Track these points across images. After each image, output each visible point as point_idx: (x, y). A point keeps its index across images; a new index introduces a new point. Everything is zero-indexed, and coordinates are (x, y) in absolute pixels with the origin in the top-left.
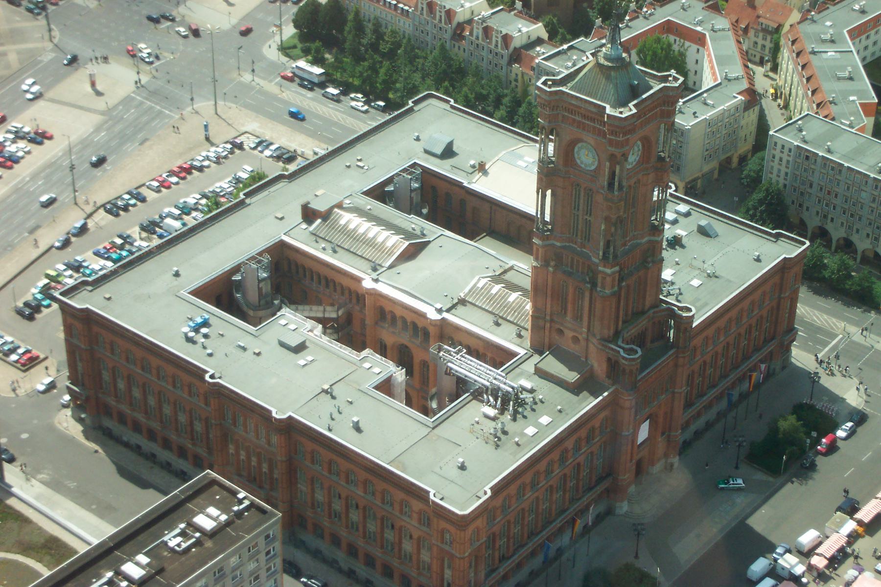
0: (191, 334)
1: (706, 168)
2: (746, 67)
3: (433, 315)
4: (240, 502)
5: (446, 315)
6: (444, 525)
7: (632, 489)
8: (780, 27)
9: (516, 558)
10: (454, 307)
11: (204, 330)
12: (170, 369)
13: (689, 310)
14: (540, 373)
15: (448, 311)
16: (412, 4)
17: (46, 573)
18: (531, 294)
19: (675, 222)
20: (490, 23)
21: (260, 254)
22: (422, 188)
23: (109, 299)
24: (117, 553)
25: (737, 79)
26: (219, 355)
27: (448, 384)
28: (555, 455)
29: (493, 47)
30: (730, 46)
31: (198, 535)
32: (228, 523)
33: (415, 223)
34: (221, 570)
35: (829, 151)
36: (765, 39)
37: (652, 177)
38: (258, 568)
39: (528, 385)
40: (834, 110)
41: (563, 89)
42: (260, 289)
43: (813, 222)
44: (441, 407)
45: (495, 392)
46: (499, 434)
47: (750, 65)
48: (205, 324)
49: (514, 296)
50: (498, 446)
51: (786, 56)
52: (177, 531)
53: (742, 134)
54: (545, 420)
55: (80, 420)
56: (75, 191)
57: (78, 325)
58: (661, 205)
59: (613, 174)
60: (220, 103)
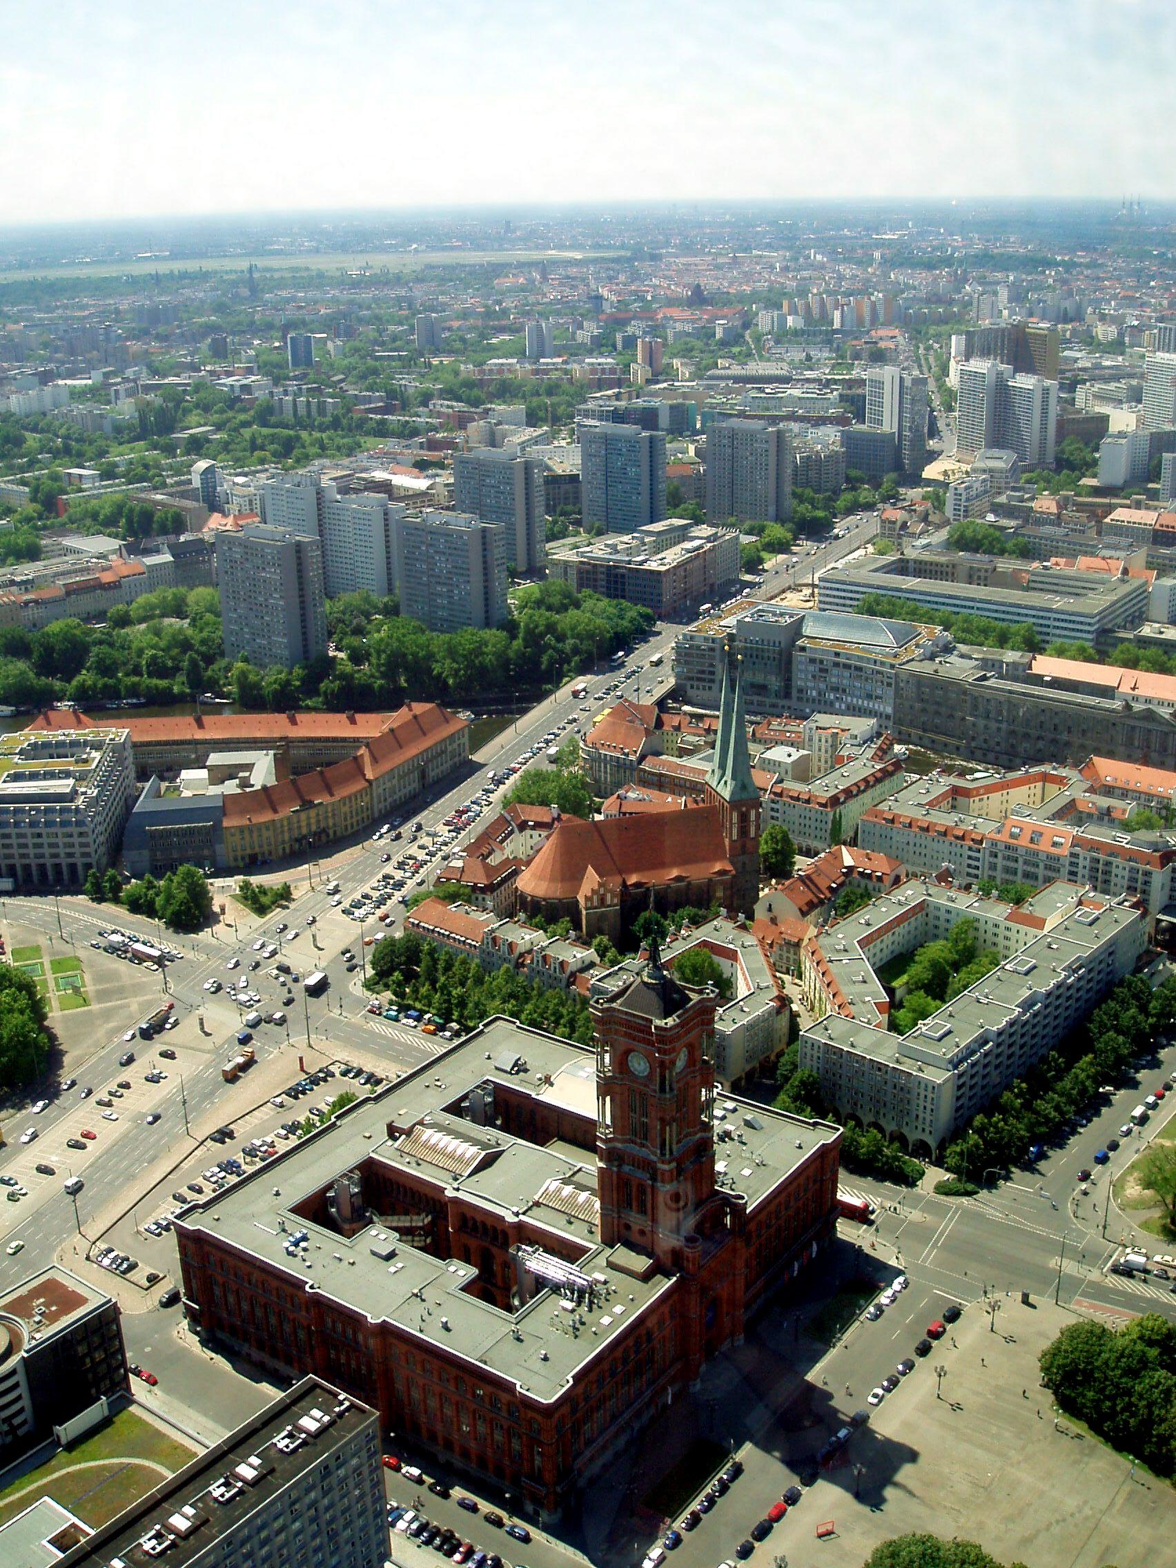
0: (292, 1249)
1: (748, 1068)
2: (775, 976)
3: (511, 1219)
4: (341, 1403)
5: (522, 1217)
6: (530, 1414)
7: (703, 1368)
8: (801, 940)
9: (601, 1441)
10: (530, 1209)
11: (303, 1244)
12: (275, 1283)
13: (743, 1198)
14: (612, 1266)
15: (524, 1213)
16: (479, 939)
17: (170, 1476)
18: (599, 1193)
19: (724, 1118)
20: (547, 952)
21: (351, 1171)
22: (495, 1102)
23: (218, 1220)
24: (231, 1456)
25: (767, 987)
26: (318, 1268)
27: (529, 1282)
28: (631, 1342)
29: (552, 972)
30: (760, 960)
31: (303, 1436)
32: (332, 1423)
33: (490, 1134)
34: (326, 1468)
35: (852, 1046)
36: (788, 952)
37: (698, 1079)
38: (360, 1466)
39: (602, 1278)
40: (853, 1010)
41: (614, 1005)
42: (352, 1204)
43: (846, 1109)
44: (523, 1304)
45: (570, 1286)
46: (578, 1325)
47: (778, 974)
48: (304, 1238)
49: (583, 1196)
50: (576, 1337)
51: (807, 964)
52: (285, 1433)
53: (776, 1037)
54: (618, 1309)
55: (197, 1333)
56: (187, 1123)
57: (190, 1244)
58: (711, 1102)
59: (663, 1078)
60: (313, 1036)
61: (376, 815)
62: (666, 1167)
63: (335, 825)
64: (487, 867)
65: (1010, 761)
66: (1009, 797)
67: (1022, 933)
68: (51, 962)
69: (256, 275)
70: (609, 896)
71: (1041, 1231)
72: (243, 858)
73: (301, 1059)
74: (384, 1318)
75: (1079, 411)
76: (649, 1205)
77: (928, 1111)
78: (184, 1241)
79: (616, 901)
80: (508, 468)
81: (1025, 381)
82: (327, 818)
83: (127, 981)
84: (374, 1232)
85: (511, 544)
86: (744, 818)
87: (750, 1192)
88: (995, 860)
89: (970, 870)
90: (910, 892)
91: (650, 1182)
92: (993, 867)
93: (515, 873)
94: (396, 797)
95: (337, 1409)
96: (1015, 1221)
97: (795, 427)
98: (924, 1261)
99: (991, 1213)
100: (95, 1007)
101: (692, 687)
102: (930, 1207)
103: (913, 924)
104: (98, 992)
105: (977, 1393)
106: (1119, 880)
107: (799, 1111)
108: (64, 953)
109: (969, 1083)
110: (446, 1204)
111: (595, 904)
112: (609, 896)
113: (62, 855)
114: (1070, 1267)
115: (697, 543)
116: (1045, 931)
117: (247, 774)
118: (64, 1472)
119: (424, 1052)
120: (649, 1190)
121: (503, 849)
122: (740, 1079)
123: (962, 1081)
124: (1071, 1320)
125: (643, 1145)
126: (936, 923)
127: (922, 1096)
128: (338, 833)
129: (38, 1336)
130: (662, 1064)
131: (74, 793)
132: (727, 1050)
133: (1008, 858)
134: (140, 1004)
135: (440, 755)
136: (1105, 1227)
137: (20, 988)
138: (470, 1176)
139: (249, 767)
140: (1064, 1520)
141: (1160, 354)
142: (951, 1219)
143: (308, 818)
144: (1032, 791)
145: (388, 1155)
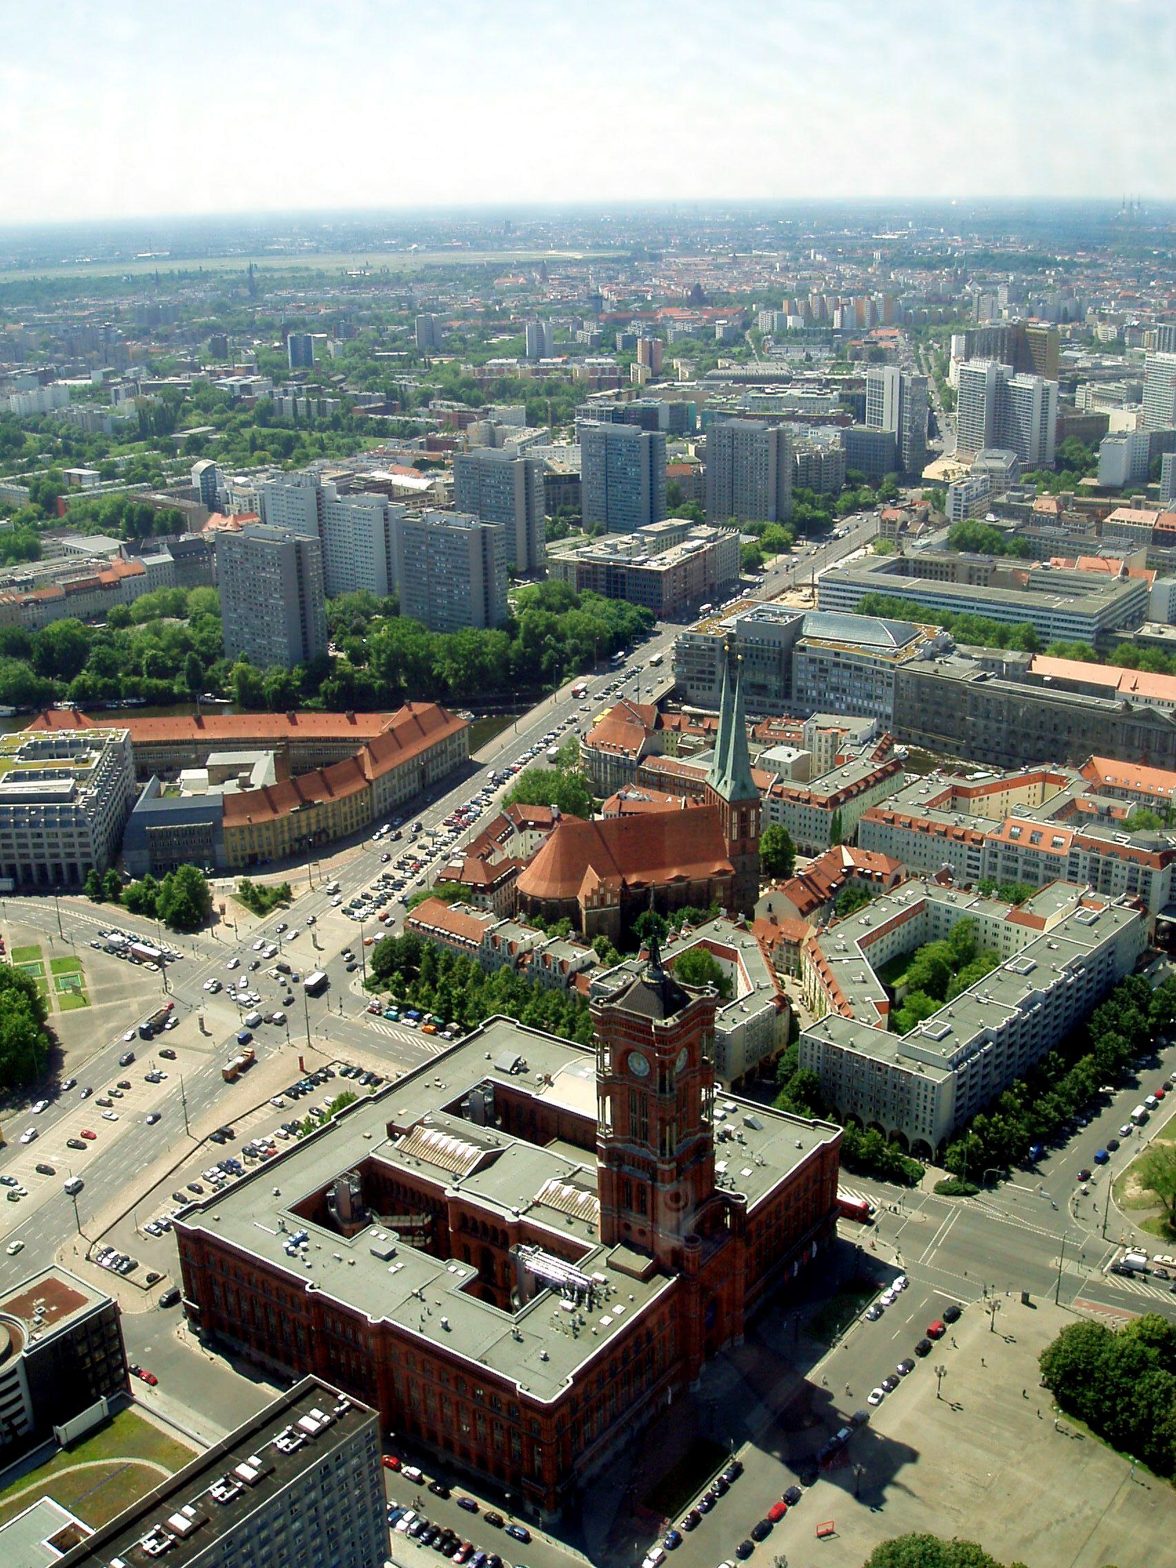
0: (292, 1249)
1: (748, 1068)
2: (775, 976)
3: (511, 1219)
4: (341, 1403)
5: (522, 1217)
6: (530, 1414)
7: (703, 1368)
8: (801, 940)
9: (601, 1441)
10: (530, 1209)
11: (303, 1244)
12: (275, 1283)
13: (743, 1198)
14: (612, 1266)
15: (524, 1213)
16: (479, 939)
17: (170, 1476)
18: (599, 1193)
19: (724, 1118)
20: (547, 952)
21: (351, 1171)
22: (495, 1102)
23: (218, 1220)
25: (767, 987)
26: (318, 1268)
27: (529, 1282)
28: (631, 1342)
29: (552, 972)
30: (760, 960)
31: (303, 1436)
32: (332, 1423)
33: (490, 1134)
34: (326, 1468)
35: (852, 1046)
36: (788, 952)
37: (698, 1079)
38: (360, 1466)
39: (602, 1278)
40: (853, 1010)
41: (614, 1005)
42: (352, 1204)
43: (846, 1109)
44: (523, 1304)
45: (570, 1286)
46: (578, 1325)
47: (778, 974)
48: (304, 1238)
49: (583, 1196)
50: (576, 1337)
51: (807, 964)
52: (285, 1433)
53: (776, 1037)
54: (618, 1309)
55: (197, 1333)
56: (187, 1123)
57: (190, 1244)
58: (711, 1102)
59: (663, 1078)
60: (313, 1036)
61: (376, 815)
62: (666, 1167)
63: (335, 825)
64: (487, 867)
65: (1010, 761)
66: (1009, 797)
67: (1022, 933)
68: (51, 962)
69: (256, 275)
70: (609, 896)
71: (1041, 1231)
72: (243, 858)
73: (301, 1059)
74: (384, 1318)
75: (1079, 411)
76: (649, 1205)
77: (928, 1111)
78: (184, 1241)
79: (616, 901)
80: (508, 468)
81: (1025, 381)
82: (327, 818)
83: (127, 981)
84: (374, 1232)
85: (511, 544)
86: (744, 818)
87: (750, 1192)
88: (995, 860)
89: (970, 870)
90: (910, 892)
91: (650, 1182)
92: (993, 867)
93: (515, 873)
94: (396, 797)
95: (337, 1409)
96: (1015, 1221)
97: (795, 427)
98: (924, 1261)
99: (991, 1213)
100: (95, 1007)
101: (692, 687)
102: (930, 1207)
103: (913, 924)
104: (98, 992)
105: (977, 1393)
106: (1119, 880)
107: (799, 1111)
108: (64, 953)
109: (969, 1083)
110: (446, 1204)
111: (595, 904)
112: (609, 896)
113: (62, 855)
114: (1070, 1267)
115: (697, 543)
116: (1045, 931)
117: (247, 774)
118: (64, 1472)
119: (424, 1052)
120: (649, 1190)
121: (503, 849)
122: (740, 1079)
123: (962, 1081)
124: (1071, 1320)
125: (643, 1145)
126: (936, 923)
127: (922, 1096)
128: (338, 833)
129: (38, 1336)
130: (662, 1064)
131: (74, 793)
132: (727, 1050)
133: (1008, 858)
134: (140, 1004)
135: (440, 755)
136: (1105, 1227)
137: (20, 988)
138: (470, 1176)
139: (249, 767)
140: (1064, 1520)
141: (1160, 354)
142: (951, 1219)
143: (308, 818)
144: (1032, 791)
145: (388, 1155)
